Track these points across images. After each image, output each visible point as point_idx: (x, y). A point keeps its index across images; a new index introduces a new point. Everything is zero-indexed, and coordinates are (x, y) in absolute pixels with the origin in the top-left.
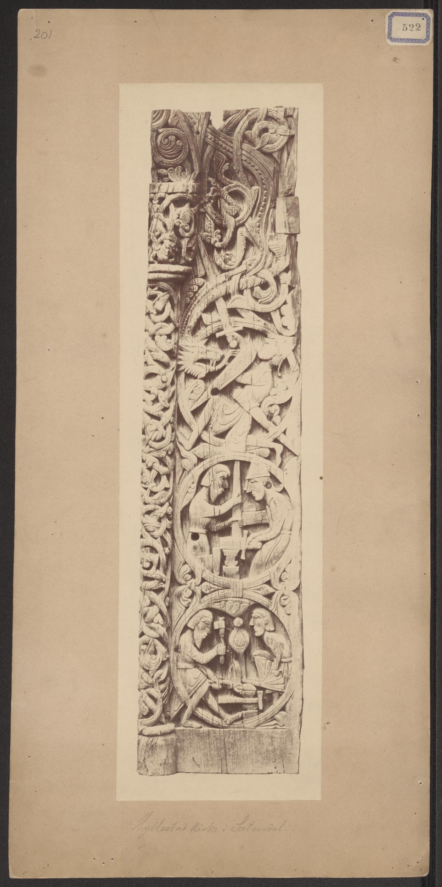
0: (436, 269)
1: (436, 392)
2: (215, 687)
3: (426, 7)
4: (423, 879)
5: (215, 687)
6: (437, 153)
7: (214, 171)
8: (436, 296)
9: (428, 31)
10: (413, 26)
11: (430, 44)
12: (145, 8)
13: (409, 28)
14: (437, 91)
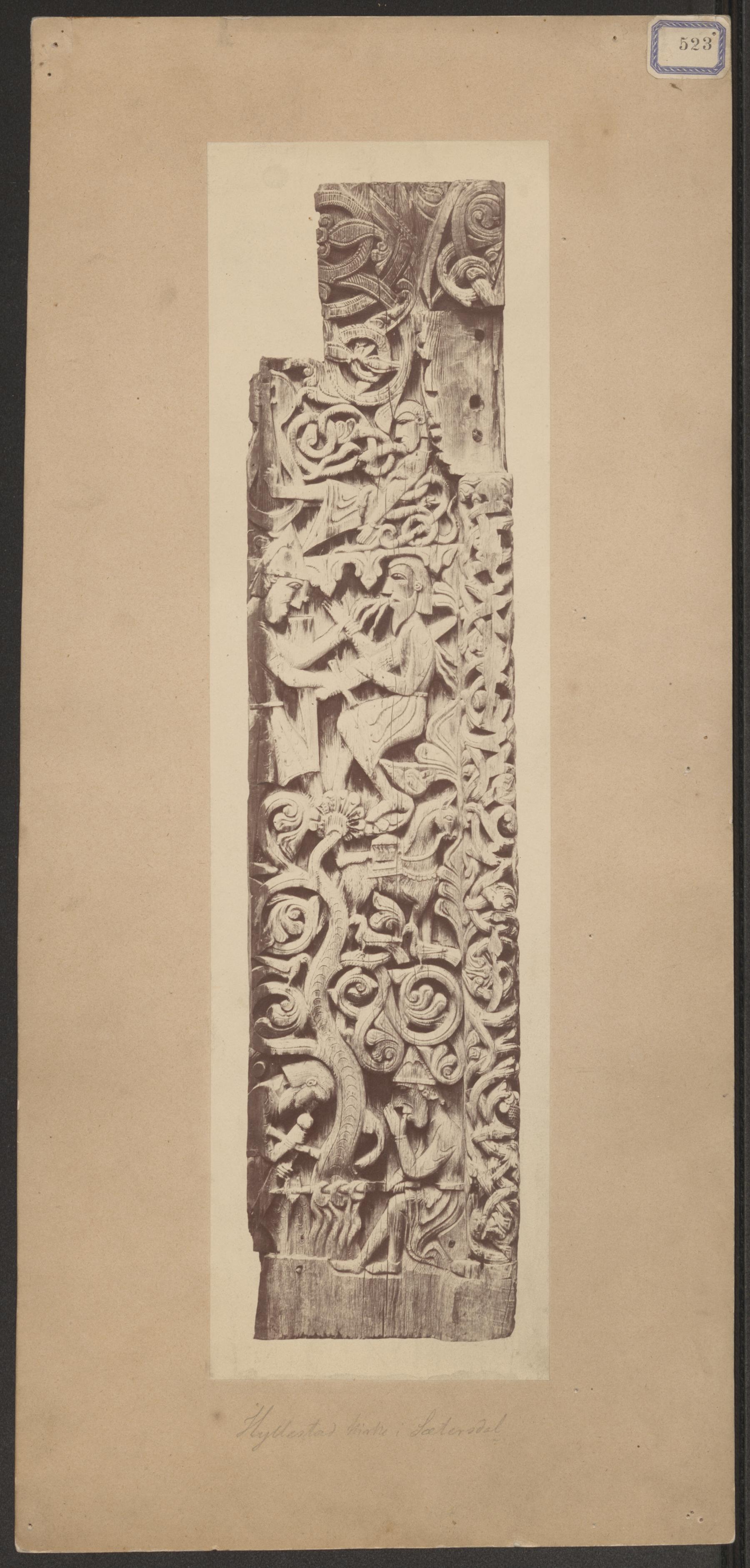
0: (742, 413)
1: (742, 631)
2: (362, 1184)
3: (718, 12)
4: (724, 1548)
5: (362, 1184)
6: (742, 207)
7: (407, 267)
8: (742, 460)
9: (722, 54)
10: (698, 41)
11: (726, 74)
12: (21, 590)
13: (691, 45)
14: (742, 98)
